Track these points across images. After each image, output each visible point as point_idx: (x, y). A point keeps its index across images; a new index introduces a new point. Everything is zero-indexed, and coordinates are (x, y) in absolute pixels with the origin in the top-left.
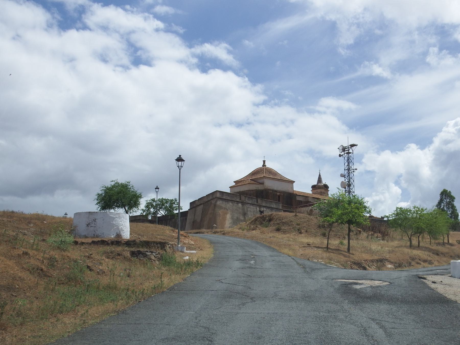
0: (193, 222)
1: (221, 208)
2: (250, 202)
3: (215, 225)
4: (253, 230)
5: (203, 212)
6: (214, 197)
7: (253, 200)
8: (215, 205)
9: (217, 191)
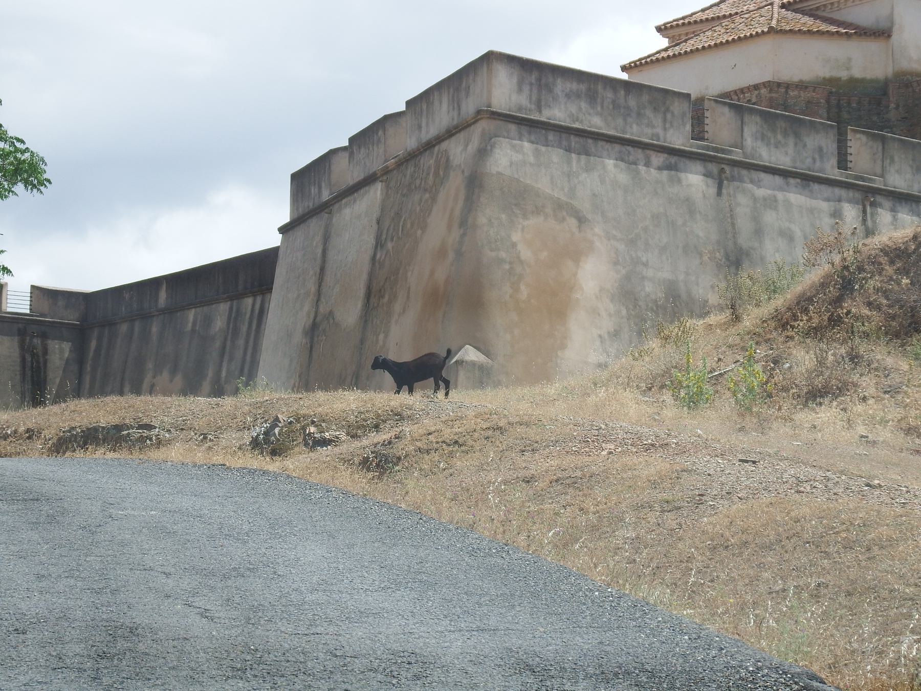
0: (313, 330)
1: (520, 199)
2: (782, 158)
3: (470, 354)
4: (815, 395)
5: (379, 244)
6: (469, 107)
7: (813, 141)
8: (475, 182)
9: (490, 58)
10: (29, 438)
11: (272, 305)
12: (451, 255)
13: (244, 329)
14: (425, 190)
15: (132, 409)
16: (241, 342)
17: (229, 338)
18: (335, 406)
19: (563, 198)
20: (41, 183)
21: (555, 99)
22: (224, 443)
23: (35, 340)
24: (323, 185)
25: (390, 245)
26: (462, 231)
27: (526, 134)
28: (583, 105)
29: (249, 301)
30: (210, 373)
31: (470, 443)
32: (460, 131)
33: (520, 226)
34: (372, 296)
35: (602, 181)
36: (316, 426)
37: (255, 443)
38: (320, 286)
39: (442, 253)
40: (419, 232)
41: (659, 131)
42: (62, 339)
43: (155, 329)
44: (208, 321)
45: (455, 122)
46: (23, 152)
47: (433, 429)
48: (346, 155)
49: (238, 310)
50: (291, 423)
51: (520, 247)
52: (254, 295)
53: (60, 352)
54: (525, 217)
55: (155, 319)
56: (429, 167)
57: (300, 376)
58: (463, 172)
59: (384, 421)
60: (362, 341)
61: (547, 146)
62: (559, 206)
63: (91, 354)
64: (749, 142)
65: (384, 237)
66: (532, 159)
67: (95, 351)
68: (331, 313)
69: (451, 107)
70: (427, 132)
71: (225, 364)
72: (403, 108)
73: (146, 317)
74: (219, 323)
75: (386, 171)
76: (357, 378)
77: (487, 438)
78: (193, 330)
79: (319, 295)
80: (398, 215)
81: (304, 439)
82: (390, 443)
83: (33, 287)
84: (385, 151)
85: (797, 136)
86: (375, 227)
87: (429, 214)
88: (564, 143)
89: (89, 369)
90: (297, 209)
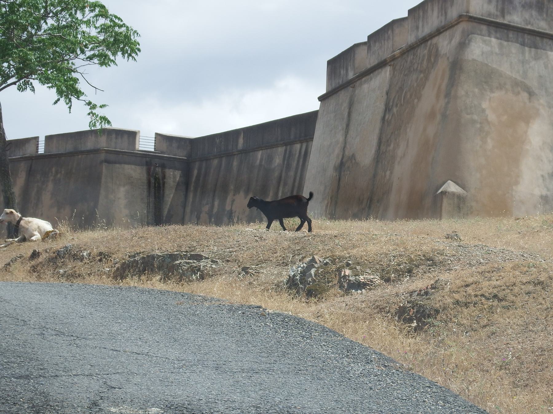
1: (488, 78)
3: (451, 187)
5: (388, 109)
6: (453, 13)
8: (456, 66)
10: (100, 260)
11: (313, 149)
12: (439, 117)
13: (294, 164)
14: (421, 72)
15: (188, 238)
16: (292, 173)
17: (284, 170)
18: (369, 249)
19: (519, 78)
20: (133, 51)
21: (514, 8)
22: (262, 277)
23: (157, 169)
24: (349, 68)
25: (395, 110)
26: (446, 100)
27: (493, 32)
28: (534, 13)
29: (298, 146)
31: (511, 298)
32: (446, 30)
33: (488, 97)
34: (382, 145)
35: (546, 67)
36: (351, 269)
37: (292, 283)
38: (346, 137)
39: (432, 115)
40: (416, 101)
42: (175, 168)
43: (235, 163)
44: (270, 159)
45: (443, 24)
46: (120, 26)
47: (470, 280)
48: (366, 48)
49: (290, 152)
50: (326, 264)
51: (488, 112)
52: (301, 142)
53: (173, 176)
54: (492, 91)
55: (235, 156)
56: (424, 56)
57: (331, 198)
58: (448, 58)
59: (417, 266)
61: (508, 41)
62: (516, 84)
63: (194, 179)
65: (391, 104)
66: (497, 50)
67: (196, 177)
68: (353, 156)
69: (440, 14)
70: (423, 31)
71: (281, 189)
72: (406, 15)
73: (230, 155)
74: (278, 160)
75: (393, 58)
76: (371, 201)
77: (528, 293)
78: (260, 165)
79: (345, 143)
80: (401, 89)
81: (340, 281)
82: (426, 293)
83: (156, 134)
84: (393, 45)
86: (385, 97)
87: (423, 88)
88: (520, 39)
89: (192, 189)
90: (331, 85)
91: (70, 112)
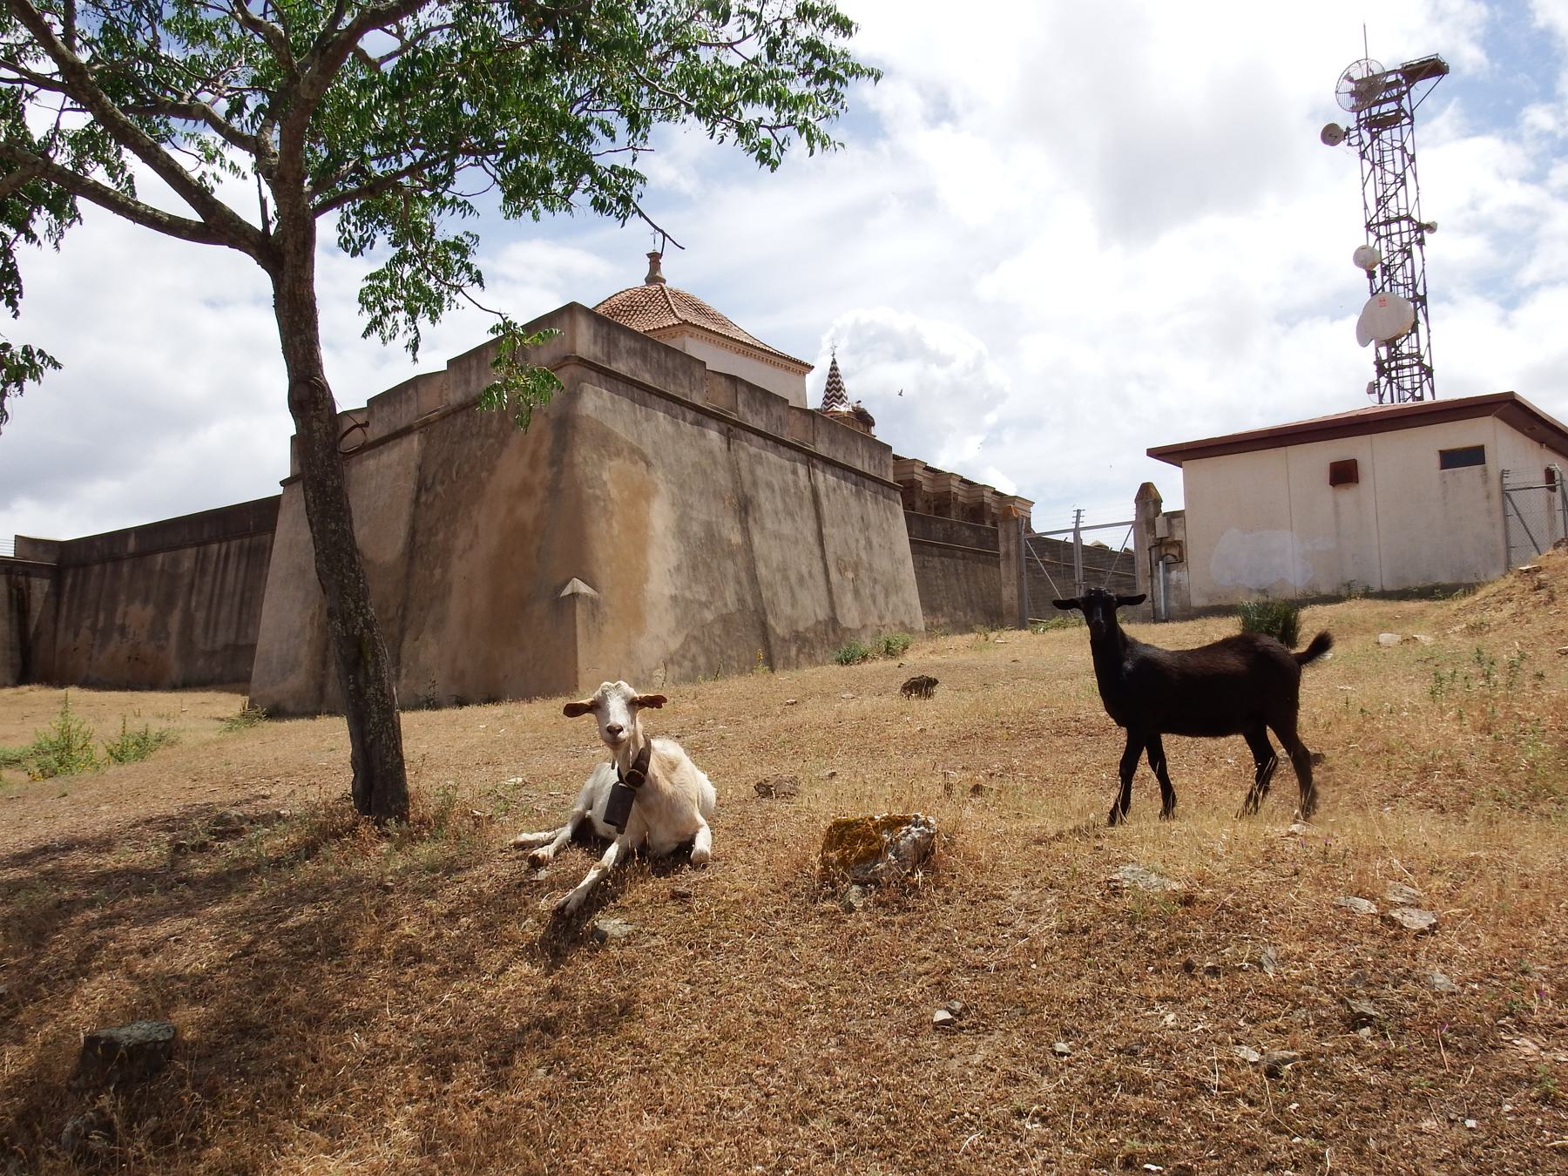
1: (605, 441)
5: (422, 486)
12: (540, 494)
13: (211, 568)
16: (209, 579)
29: (215, 547)
30: (180, 603)
41: (687, 390)
42: (43, 577)
44: (176, 563)
51: (610, 485)
52: (220, 542)
53: (40, 587)
60: (408, 576)
63: (67, 588)
64: (741, 408)
73: (117, 560)
75: (426, 424)
78: (162, 570)
85: (768, 406)
91: (415, 360)
